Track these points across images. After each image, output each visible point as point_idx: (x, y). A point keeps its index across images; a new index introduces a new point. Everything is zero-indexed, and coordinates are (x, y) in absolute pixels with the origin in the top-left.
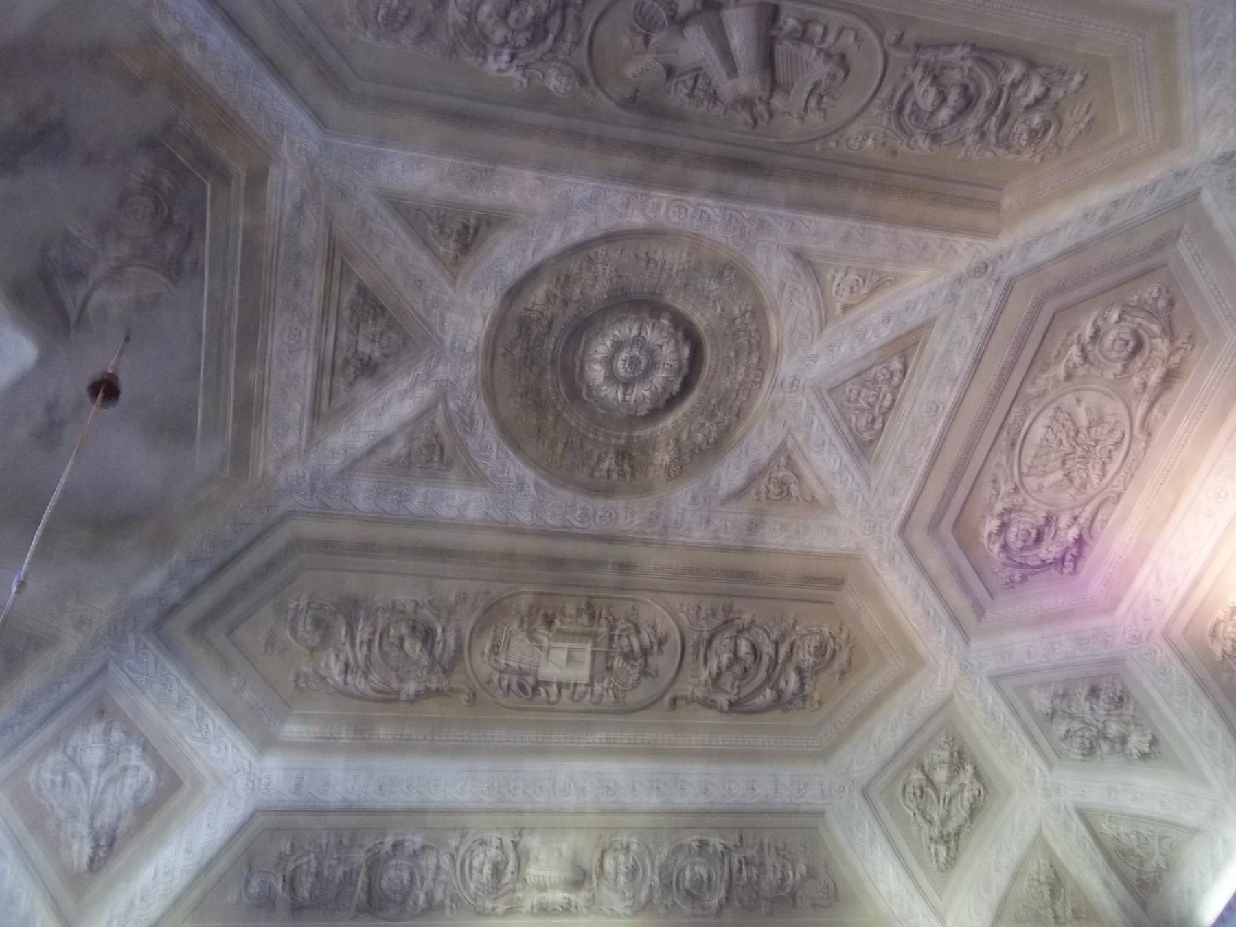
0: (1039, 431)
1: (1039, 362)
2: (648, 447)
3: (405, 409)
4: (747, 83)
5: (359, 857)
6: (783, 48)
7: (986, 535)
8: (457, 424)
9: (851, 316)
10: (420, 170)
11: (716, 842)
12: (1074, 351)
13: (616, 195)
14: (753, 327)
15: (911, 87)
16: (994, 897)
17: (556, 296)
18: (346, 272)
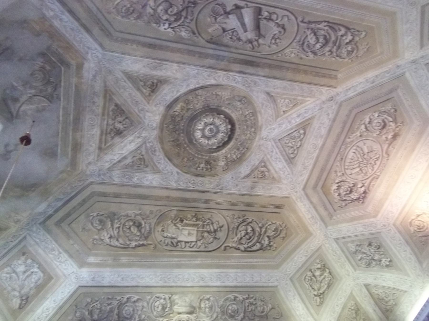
0: (351, 155)
1: (351, 130)
3: (132, 147)
4: (250, 35)
5: (115, 303)
6: (263, 23)
8: (150, 151)
10: (136, 64)
12: (363, 126)
13: (206, 73)
15: (307, 36)
17: (184, 107)
18: (111, 100)
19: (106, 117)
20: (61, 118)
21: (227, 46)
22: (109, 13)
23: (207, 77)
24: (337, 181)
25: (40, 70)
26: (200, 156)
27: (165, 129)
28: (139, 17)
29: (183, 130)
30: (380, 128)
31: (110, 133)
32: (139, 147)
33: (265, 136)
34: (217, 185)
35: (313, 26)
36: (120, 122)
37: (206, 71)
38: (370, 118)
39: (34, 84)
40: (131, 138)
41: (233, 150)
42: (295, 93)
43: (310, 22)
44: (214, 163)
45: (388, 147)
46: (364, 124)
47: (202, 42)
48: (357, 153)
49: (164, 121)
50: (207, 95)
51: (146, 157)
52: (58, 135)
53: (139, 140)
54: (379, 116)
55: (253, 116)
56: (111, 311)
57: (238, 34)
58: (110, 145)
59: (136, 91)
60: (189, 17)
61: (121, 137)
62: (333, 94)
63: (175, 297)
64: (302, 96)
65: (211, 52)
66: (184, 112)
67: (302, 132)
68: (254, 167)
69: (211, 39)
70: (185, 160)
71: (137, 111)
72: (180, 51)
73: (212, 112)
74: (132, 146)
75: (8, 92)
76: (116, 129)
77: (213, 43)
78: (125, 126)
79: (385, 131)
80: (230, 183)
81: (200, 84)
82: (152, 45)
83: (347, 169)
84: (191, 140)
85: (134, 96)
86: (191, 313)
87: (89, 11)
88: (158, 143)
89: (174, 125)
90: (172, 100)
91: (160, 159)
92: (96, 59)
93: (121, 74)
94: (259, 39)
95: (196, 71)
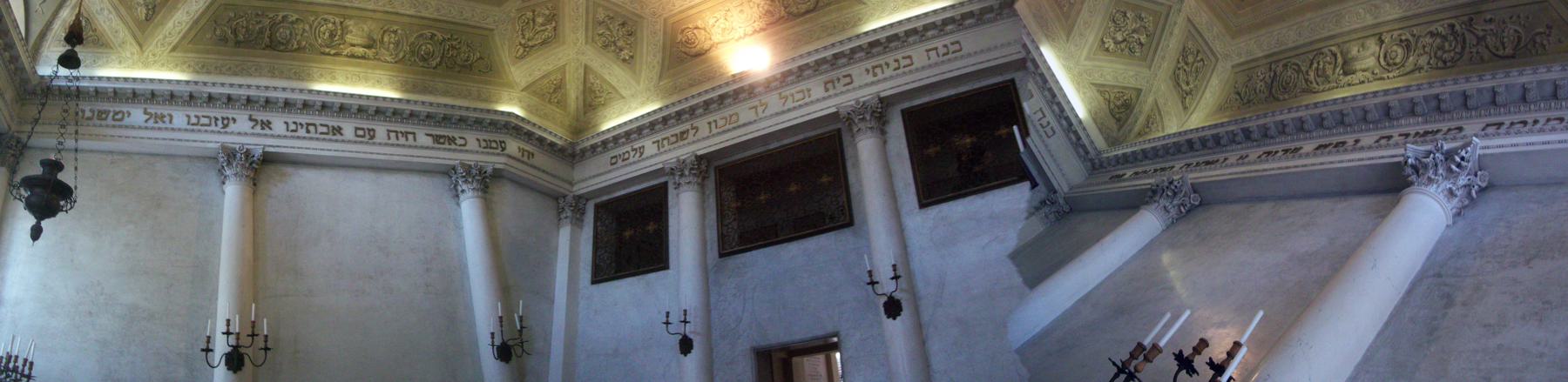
5: (266, 22)
11: (439, 36)
16: (531, 79)
56: (261, 31)
63: (349, 23)
86: (369, 47)
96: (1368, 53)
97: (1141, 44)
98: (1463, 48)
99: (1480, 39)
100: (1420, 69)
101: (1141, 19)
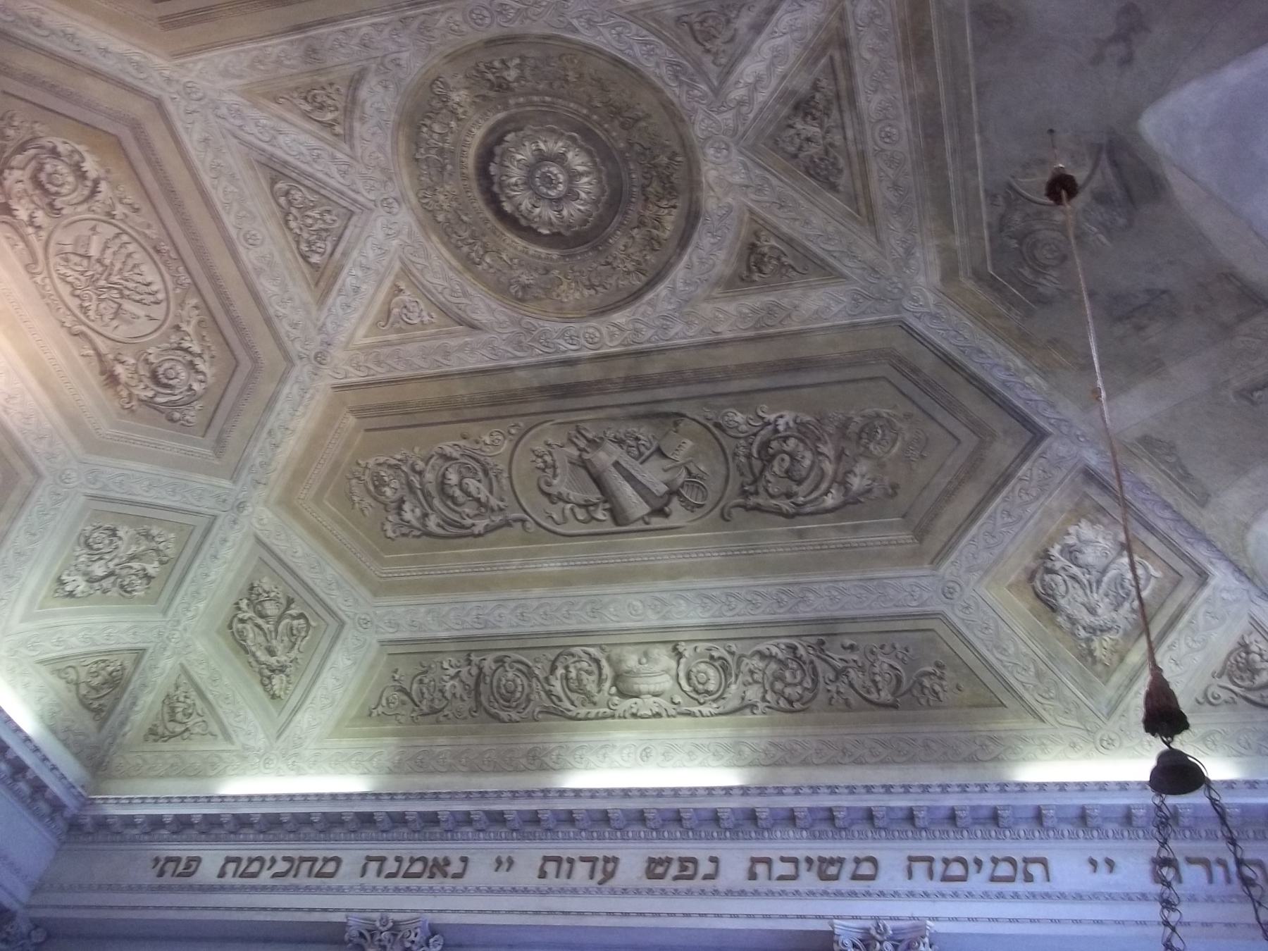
0: (149, 273)
1: (209, 322)
2: (481, 102)
3: (750, 69)
4: (604, 458)
6: (595, 496)
7: (86, 155)
8: (691, 70)
9: (387, 284)
10: (817, 307)
12: (196, 348)
13: (648, 337)
14: (466, 249)
15: (491, 492)
17: (655, 228)
18: (852, 199)
19: (852, 149)
20: (977, 138)
21: (635, 418)
22: (908, 416)
23: (639, 326)
24: (103, 186)
25: (1045, 267)
26: (535, 98)
27: (678, 149)
28: (844, 426)
29: (626, 161)
30: (161, 371)
31: (829, 102)
32: (729, 73)
33: (395, 210)
34: (424, 29)
35: (498, 519)
36: (808, 140)
37: (649, 341)
38: (203, 373)
39: (1055, 234)
40: (761, 96)
41: (454, 144)
42: (411, 347)
43: (507, 524)
44: (484, 92)
45: (95, 349)
46: (200, 355)
47: (689, 409)
48: (142, 288)
49: (690, 170)
50: (615, 277)
51: (696, 50)
52: (977, 88)
53: (737, 94)
54: (190, 389)
55: (468, 254)
57: (628, 452)
58: (817, 60)
59: (795, 235)
60: (743, 459)
61: (794, 93)
62: (326, 370)
64: (389, 344)
65: (662, 393)
66: (647, 213)
67: (315, 259)
68: (357, 114)
69: (676, 424)
70: (572, 76)
71: (774, 182)
72: (729, 374)
73: (577, 233)
74: (749, 70)
75: (1121, 221)
76: (814, 119)
77: (667, 415)
78: (792, 132)
79: (144, 370)
80: (393, 48)
81: (649, 303)
82: (798, 369)
83: (117, 236)
84: (587, 137)
85: (796, 220)
87: (952, 407)
88: (675, 100)
89: (655, 166)
90: (696, 236)
91: (650, 53)
92: (915, 294)
93: (846, 271)
94: (580, 456)
95: (672, 332)
96: (657, 668)
97: (148, 578)
98: (815, 682)
99: (840, 673)
100: (753, 706)
101: (148, 536)
